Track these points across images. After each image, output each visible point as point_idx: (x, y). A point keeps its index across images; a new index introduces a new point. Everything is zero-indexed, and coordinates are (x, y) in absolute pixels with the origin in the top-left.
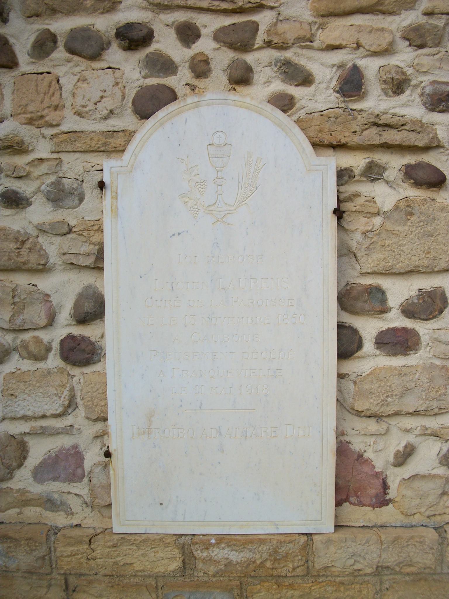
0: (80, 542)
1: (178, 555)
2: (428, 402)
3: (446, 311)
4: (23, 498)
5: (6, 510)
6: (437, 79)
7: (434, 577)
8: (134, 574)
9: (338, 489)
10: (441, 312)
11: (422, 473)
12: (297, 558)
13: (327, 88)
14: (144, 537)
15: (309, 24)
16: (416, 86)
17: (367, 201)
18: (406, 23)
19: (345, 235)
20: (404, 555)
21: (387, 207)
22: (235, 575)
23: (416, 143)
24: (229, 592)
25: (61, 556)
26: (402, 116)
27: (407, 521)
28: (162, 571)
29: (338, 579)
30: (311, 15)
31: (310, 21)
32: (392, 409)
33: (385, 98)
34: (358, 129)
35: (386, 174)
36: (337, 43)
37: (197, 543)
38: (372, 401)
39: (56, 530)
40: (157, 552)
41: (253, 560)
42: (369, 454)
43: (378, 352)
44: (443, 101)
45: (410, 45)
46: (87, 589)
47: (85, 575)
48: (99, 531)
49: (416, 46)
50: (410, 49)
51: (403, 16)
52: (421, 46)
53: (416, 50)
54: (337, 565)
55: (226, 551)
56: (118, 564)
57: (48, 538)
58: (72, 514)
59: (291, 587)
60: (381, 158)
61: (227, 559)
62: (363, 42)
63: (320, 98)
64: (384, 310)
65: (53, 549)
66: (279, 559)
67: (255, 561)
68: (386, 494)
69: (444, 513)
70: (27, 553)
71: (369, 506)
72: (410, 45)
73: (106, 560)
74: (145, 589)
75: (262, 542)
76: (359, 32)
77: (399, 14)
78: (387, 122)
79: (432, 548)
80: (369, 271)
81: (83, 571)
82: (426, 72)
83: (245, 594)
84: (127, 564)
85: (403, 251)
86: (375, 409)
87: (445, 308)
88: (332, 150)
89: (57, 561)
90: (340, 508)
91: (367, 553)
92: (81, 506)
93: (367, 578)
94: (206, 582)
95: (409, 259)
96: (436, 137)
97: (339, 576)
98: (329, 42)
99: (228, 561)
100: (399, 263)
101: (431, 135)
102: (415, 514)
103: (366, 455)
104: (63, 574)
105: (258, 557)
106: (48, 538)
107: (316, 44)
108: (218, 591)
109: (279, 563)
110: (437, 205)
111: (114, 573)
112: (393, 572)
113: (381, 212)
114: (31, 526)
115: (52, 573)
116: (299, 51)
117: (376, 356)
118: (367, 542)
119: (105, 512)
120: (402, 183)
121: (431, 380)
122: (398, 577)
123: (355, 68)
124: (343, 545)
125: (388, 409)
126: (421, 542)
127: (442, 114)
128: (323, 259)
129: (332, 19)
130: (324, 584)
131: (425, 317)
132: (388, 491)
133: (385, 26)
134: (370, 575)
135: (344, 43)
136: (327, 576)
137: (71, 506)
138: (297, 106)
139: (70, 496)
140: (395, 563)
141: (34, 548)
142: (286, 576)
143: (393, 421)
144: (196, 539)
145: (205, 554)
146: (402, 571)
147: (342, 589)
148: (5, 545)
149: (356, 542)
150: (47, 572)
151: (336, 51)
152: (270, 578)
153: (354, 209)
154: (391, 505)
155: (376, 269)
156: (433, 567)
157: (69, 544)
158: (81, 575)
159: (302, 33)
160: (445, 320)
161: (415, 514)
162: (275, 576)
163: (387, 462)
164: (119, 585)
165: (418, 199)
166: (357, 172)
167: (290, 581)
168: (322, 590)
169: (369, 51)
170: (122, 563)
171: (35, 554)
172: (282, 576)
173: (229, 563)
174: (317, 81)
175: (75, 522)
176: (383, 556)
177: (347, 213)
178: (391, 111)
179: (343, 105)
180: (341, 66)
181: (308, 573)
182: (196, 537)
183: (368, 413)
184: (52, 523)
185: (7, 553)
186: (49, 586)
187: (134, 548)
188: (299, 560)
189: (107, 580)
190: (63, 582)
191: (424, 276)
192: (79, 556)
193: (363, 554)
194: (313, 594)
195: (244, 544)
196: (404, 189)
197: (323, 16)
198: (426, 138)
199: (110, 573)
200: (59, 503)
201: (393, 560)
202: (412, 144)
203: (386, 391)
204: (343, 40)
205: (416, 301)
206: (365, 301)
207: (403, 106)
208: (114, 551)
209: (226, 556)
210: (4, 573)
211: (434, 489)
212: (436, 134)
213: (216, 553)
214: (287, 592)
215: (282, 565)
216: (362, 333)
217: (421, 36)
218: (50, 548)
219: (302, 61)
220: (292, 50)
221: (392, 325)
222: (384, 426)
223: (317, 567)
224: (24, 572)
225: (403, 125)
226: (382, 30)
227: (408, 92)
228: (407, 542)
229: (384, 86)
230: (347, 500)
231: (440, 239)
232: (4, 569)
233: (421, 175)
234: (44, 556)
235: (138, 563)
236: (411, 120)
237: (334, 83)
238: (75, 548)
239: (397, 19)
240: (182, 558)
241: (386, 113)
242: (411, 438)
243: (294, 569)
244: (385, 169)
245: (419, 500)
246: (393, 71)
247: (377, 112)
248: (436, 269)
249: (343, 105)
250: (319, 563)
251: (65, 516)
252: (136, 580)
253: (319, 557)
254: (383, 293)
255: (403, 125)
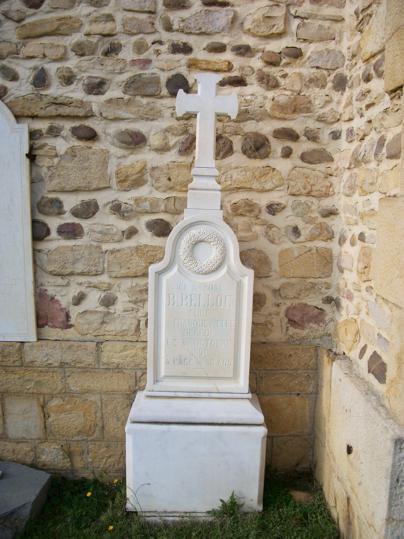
2: (89, 267)
3: (98, 213)
6: (91, 75)
7: (95, 370)
9: (38, 317)
10: (94, 214)
11: (90, 310)
12: (15, 356)
13: (27, 82)
15: (16, 44)
16: (80, 80)
17: (50, 149)
18: (74, 41)
19: (386, 115)
20: (76, 356)
21: (62, 152)
23: (78, 114)
26: (71, 98)
27: (82, 338)
29: (39, 369)
30: (17, 38)
31: (16, 42)
32: (68, 271)
33: (61, 87)
34: (43, 106)
35: (62, 133)
36: (32, 55)
38: (56, 265)
42: (58, 297)
43: (60, 237)
44: (95, 88)
45: (76, 54)
49: (79, 55)
50: (76, 57)
51: (73, 36)
52: (83, 55)
53: (80, 57)
54: (38, 360)
60: (58, 123)
62: (47, 54)
63: (23, 88)
64: (60, 212)
66: (6, 356)
68: (68, 321)
72: (76, 54)
76: (44, 48)
77: (71, 35)
78: (61, 102)
79: (92, 353)
80: (51, 190)
82: (85, 71)
85: (70, 178)
86: (58, 270)
87: (97, 211)
88: (31, 119)
93: (56, 369)
95: (74, 183)
96: (91, 110)
97: (39, 367)
98: (27, 54)
100: (67, 185)
101: (88, 109)
103: (56, 298)
107: (21, 56)
109: (6, 358)
110: (92, 151)
113: (59, 155)
116: (11, 60)
117: (59, 239)
120: (72, 138)
121: (90, 254)
122: (74, 369)
123: (43, 69)
124: (40, 348)
125: (66, 270)
127: (96, 96)
128: (21, 183)
129: (30, 40)
131: (84, 217)
132: (70, 319)
133: (60, 43)
134: (57, 367)
135: (36, 55)
136: (33, 367)
138: (9, 93)
140: (71, 361)
142: (10, 366)
143: (72, 278)
146: (76, 366)
147: (42, 375)
149: (48, 347)
151: (33, 59)
153: (41, 154)
154: (72, 328)
155: (55, 189)
159: (11, 49)
160: (97, 219)
163: (69, 303)
165: (79, 147)
166: (44, 131)
167: (13, 369)
168: (31, 375)
169: (50, 59)
174: (21, 78)
177: (37, 156)
178: (65, 95)
179: (36, 92)
180: (35, 68)
183: (55, 273)
188: (16, 357)
191: (86, 193)
193: (52, 354)
196: (73, 141)
197: (24, 39)
198: (84, 111)
201: (70, 358)
202: (75, 114)
203: (64, 260)
204: (35, 53)
205: (79, 207)
206: (50, 208)
207: (72, 91)
212: (92, 108)
214: (11, 376)
215: (8, 360)
216: (50, 226)
217: (82, 49)
219: (13, 66)
220: (7, 60)
221: (67, 222)
222: (66, 281)
223: (27, 361)
225: (71, 103)
226: (58, 46)
227: (75, 83)
229: (60, 80)
231: (92, 171)
233: (81, 133)
236: (76, 100)
237: (31, 79)
239: (70, 38)
241: (62, 96)
242: (83, 289)
243: (14, 362)
244: (61, 130)
246: (64, 71)
247: (55, 96)
248: (91, 189)
249: (36, 92)
250: (28, 359)
253: (27, 355)
254: (61, 203)
255: (71, 103)
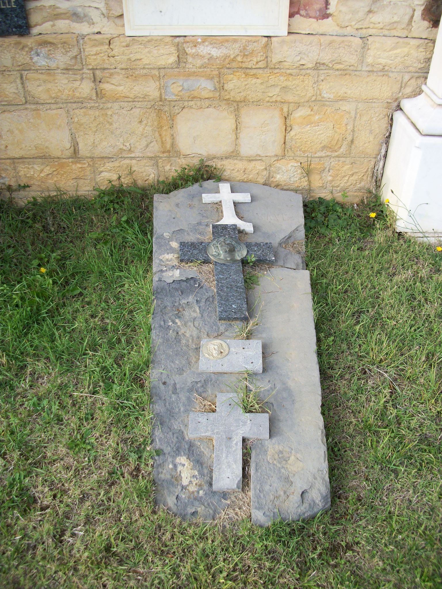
0: (102, 44)
1: (174, 52)
4: (55, 13)
5: (43, 23)
8: (143, 67)
12: (259, 54)
14: (149, 38)
20: (336, 55)
22: (215, 67)
24: (211, 80)
25: (89, 55)
28: (163, 64)
29: (289, 71)
37: (188, 42)
39: (83, 37)
40: (159, 50)
41: (228, 55)
46: (109, 80)
47: (107, 69)
48: (114, 36)
55: (209, 48)
56: (130, 60)
57: (78, 42)
58: (93, 24)
59: (255, 76)
61: (210, 54)
65: (82, 50)
66: (247, 55)
67: (229, 56)
68: (327, 9)
69: (369, 28)
70: (63, 54)
71: (314, 18)
73: (122, 57)
74: (151, 78)
75: (235, 41)
79: (356, 51)
81: (106, 66)
83: (222, 81)
84: (138, 59)
89: (86, 59)
90: (292, 19)
91: (309, 52)
92: (100, 17)
93: (308, 71)
94: (194, 73)
97: (288, 69)
99: (210, 56)
102: (347, 26)
104: (91, 69)
105: (232, 52)
106: (78, 42)
108: (203, 79)
111: (128, 67)
112: (328, 67)
114: (63, 35)
115: (83, 69)
118: (310, 44)
119: (118, 21)
122: (331, 72)
124: (293, 45)
126: (349, 46)
130: (278, 74)
132: (328, 7)
134: (311, 69)
136: (280, 69)
137: (92, 17)
139: (91, 9)
140: (329, 61)
141: (68, 50)
142: (251, 68)
144: (187, 39)
145: (194, 51)
146: (334, 67)
148: (47, 49)
150: (79, 68)
152: (240, 70)
154: (330, 19)
156: (356, 65)
157: (94, 46)
158: (105, 69)
161: (347, 26)
162: (243, 68)
164: (132, 75)
170: (134, 59)
171: (69, 54)
172: (249, 68)
173: (211, 58)
175: (96, 31)
176: (321, 55)
181: (267, 67)
182: (187, 38)
184: (79, 32)
185: (48, 55)
186: (82, 79)
187: (142, 47)
189: (123, 72)
190: (92, 75)
192: (102, 55)
194: (270, 81)
195: (222, 42)
199: (125, 67)
200: (82, 15)
208: (127, 50)
209: (209, 52)
210: (48, 71)
211: (363, 7)
213: (201, 49)
214: (252, 80)
215: (249, 60)
218: (80, 50)
223: (274, 61)
224: (62, 69)
228: (339, 45)
230: (298, 13)
232: (47, 68)
234: (77, 56)
235: (146, 58)
238: (98, 49)
240: (177, 54)
243: (257, 63)
245: (351, 15)
250: (275, 58)
251: (88, 26)
252: (145, 71)
